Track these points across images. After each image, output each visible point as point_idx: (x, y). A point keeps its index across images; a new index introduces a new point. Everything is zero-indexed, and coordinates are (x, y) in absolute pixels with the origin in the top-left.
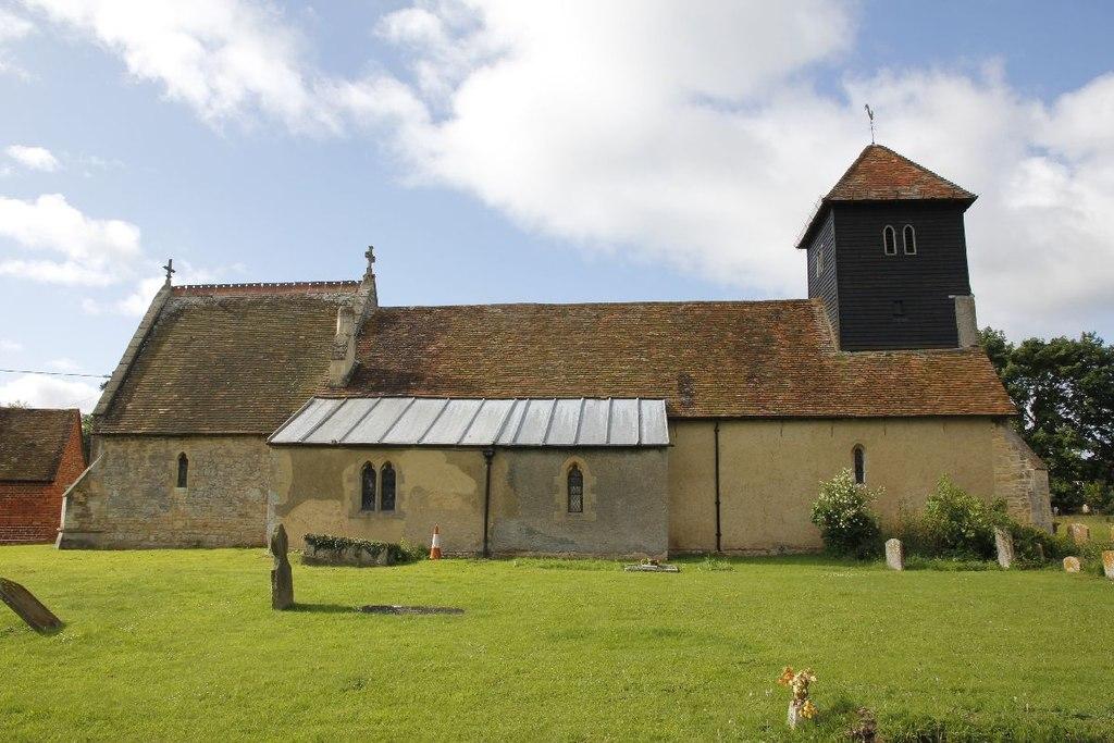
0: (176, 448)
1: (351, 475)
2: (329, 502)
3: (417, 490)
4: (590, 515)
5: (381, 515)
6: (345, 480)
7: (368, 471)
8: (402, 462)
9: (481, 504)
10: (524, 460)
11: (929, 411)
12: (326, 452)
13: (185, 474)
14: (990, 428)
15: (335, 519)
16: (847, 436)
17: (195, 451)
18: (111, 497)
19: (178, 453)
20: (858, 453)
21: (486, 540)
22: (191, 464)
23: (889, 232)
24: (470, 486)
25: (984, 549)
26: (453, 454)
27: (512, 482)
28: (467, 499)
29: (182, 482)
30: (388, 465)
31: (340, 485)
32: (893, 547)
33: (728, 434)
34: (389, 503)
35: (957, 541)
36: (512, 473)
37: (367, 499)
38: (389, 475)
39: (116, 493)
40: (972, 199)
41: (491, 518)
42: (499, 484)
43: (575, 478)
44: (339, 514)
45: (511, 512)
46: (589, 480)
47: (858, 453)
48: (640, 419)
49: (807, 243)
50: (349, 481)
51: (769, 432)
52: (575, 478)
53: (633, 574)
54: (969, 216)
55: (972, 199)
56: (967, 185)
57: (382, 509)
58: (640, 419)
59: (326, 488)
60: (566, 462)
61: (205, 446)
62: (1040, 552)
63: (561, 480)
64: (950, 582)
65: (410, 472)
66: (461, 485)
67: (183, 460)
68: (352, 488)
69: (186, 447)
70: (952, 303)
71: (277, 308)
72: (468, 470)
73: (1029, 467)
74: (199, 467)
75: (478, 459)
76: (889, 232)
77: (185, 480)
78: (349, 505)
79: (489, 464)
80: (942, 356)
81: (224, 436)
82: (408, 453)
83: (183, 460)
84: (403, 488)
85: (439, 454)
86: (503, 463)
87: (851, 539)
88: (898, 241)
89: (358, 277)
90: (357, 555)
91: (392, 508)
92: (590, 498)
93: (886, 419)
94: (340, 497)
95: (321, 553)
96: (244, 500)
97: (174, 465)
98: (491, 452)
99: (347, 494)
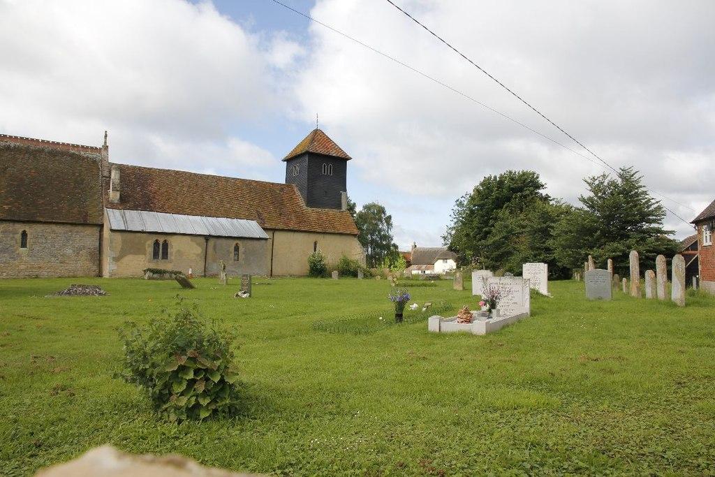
0: (20, 228)
1: (150, 243)
2: (141, 256)
6: (147, 246)
7: (157, 243)
8: (171, 240)
9: (203, 257)
10: (219, 241)
11: (349, 232)
14: (352, 238)
16: (313, 238)
17: (31, 230)
19: (21, 231)
20: (315, 244)
21: (205, 271)
23: (325, 166)
24: (199, 250)
25: (355, 275)
26: (193, 238)
28: (198, 255)
29: (24, 245)
30: (165, 241)
32: (335, 274)
33: (277, 235)
34: (165, 255)
35: (348, 271)
37: (156, 255)
38: (166, 245)
42: (210, 250)
43: (237, 248)
45: (214, 261)
46: (241, 250)
47: (315, 244)
48: (251, 228)
49: (289, 160)
51: (290, 235)
52: (237, 248)
53: (151, 281)
58: (251, 228)
59: (139, 250)
60: (234, 243)
61: (39, 228)
62: (369, 275)
63: (232, 249)
64: (349, 281)
65: (175, 245)
66: (195, 250)
67: (24, 234)
68: (150, 250)
69: (27, 228)
70: (341, 194)
71: (55, 156)
73: (43, 228)
75: (203, 240)
76: (325, 166)
78: (148, 257)
80: (332, 212)
81: (51, 223)
82: (176, 236)
83: (24, 234)
86: (211, 242)
87: (318, 271)
88: (327, 169)
89: (99, 145)
90: (171, 276)
91: (167, 258)
92: (241, 256)
93: (325, 233)
95: (155, 276)
97: (19, 237)
98: (207, 238)
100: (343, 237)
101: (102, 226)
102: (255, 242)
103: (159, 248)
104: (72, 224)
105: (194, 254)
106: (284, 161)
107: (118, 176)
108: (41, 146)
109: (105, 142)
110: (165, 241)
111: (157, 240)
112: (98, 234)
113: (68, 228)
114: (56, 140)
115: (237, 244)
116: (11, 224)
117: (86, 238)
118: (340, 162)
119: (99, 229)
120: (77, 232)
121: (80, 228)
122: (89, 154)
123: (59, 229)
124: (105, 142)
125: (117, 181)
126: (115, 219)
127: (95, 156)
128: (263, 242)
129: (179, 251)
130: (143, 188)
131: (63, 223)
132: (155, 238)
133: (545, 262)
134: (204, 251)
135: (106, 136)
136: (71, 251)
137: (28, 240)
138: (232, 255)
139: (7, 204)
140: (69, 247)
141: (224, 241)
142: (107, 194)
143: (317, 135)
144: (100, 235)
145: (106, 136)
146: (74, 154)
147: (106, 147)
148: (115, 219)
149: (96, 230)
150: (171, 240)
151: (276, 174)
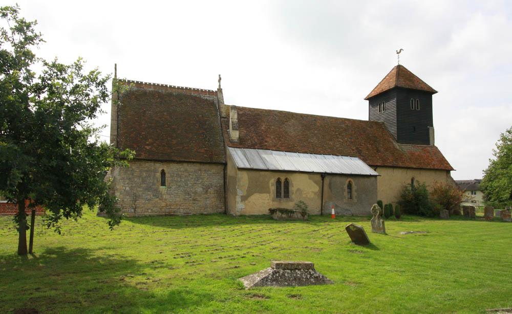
0: (160, 167)
1: (272, 181)
3: (298, 190)
4: (355, 200)
5: (285, 199)
6: (270, 185)
7: (278, 182)
8: (292, 178)
9: (320, 195)
12: (262, 173)
13: (165, 178)
15: (267, 201)
18: (125, 190)
19: (347, 182)
21: (322, 210)
22: (167, 175)
24: (316, 189)
26: (312, 176)
27: (330, 187)
28: (315, 193)
29: (163, 184)
30: (286, 179)
31: (269, 187)
36: (330, 184)
37: (278, 194)
38: (287, 183)
39: (127, 188)
40: (437, 92)
41: (324, 201)
43: (350, 186)
44: (268, 200)
46: (354, 187)
48: (356, 166)
50: (272, 185)
52: (350, 186)
54: (434, 96)
55: (437, 92)
56: (436, 89)
57: (284, 197)
58: (356, 166)
59: (263, 189)
60: (347, 181)
63: (346, 187)
65: (296, 183)
68: (273, 188)
69: (165, 167)
72: (316, 182)
74: (172, 176)
75: (319, 178)
77: (165, 182)
78: (272, 196)
79: (323, 180)
82: (297, 175)
84: (293, 189)
85: (306, 176)
86: (327, 180)
88: (415, 104)
89: (215, 89)
92: (354, 194)
93: (421, 169)
94: (269, 192)
95: (284, 216)
96: (195, 193)
97: (159, 175)
98: (323, 175)
99: (271, 191)
100: (438, 173)
101: (225, 165)
102: (366, 179)
103: (281, 186)
104: (201, 163)
105: (313, 192)
106: (367, 99)
107: (236, 116)
108: (169, 91)
109: (220, 86)
110: (286, 179)
111: (279, 179)
112: (222, 173)
113: (197, 167)
114: (173, 85)
115: (349, 182)
116: (152, 164)
117: (211, 176)
118: (426, 94)
119: (223, 168)
120: (205, 171)
121: (207, 167)
122: (207, 97)
123: (191, 168)
124: (220, 86)
125: (236, 120)
126: (240, 158)
127: (212, 99)
128: (373, 179)
129: (298, 190)
130: (266, 128)
131: (193, 162)
132: (277, 176)
133: (468, 190)
134: (321, 189)
135: (220, 79)
136: (201, 189)
137: (166, 179)
138: (346, 194)
139: (148, 145)
140: (200, 185)
141: (338, 179)
142: (228, 133)
143: (401, 71)
144: (224, 174)
145: (220, 79)
146: (196, 97)
147: (220, 90)
148: (240, 158)
149: (221, 168)
150: (292, 178)
151: (361, 112)
